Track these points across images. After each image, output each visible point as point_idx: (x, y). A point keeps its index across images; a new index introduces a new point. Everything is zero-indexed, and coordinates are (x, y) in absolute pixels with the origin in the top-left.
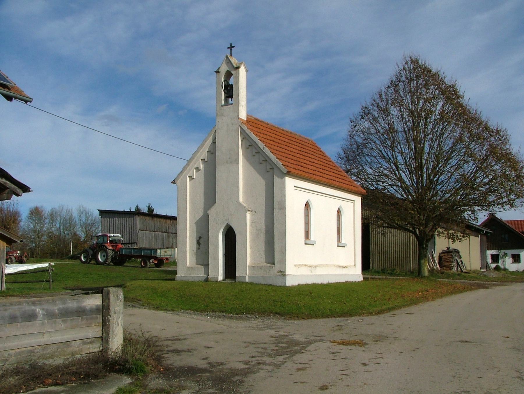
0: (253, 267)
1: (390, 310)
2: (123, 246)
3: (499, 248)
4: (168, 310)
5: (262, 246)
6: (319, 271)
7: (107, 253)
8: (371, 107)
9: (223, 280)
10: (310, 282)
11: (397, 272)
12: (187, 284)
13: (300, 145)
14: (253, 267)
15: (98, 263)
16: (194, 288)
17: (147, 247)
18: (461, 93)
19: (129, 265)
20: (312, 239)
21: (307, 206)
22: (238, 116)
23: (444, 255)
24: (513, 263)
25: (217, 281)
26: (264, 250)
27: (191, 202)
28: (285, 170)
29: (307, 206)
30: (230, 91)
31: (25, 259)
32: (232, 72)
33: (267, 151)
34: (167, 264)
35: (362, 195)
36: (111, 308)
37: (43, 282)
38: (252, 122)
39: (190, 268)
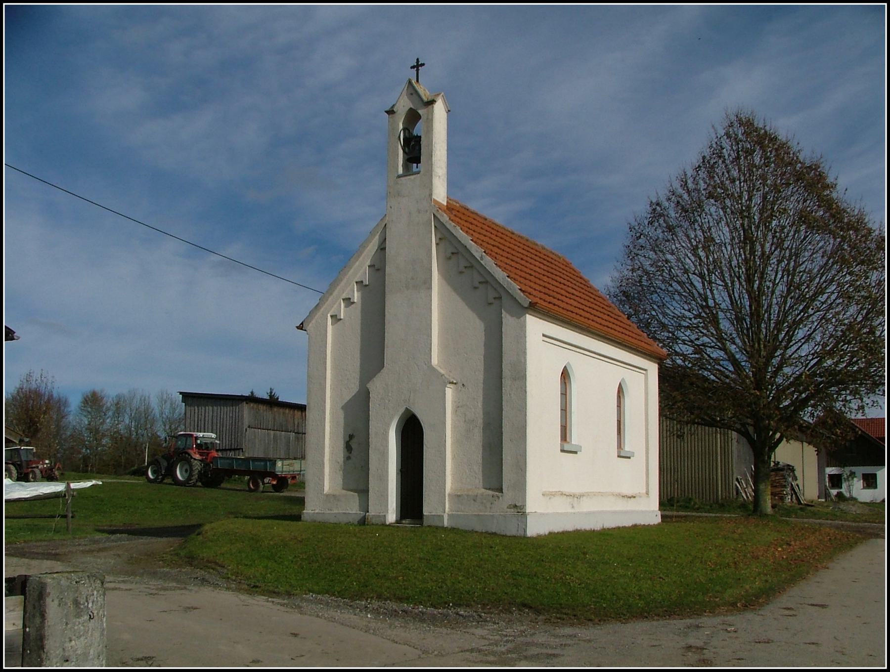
0: (459, 496)
2: (220, 454)
3: (841, 464)
4: (277, 594)
5: (477, 455)
6: (587, 506)
7: (191, 466)
8: (666, 204)
9: (397, 522)
10: (570, 528)
11: (695, 503)
12: (326, 529)
13: (545, 262)
14: (457, 497)
15: (177, 482)
16: (339, 540)
17: (261, 455)
18: (830, 180)
19: (228, 486)
21: (565, 375)
22: (431, 195)
24: (864, 488)
25: (384, 525)
26: (480, 461)
27: (335, 367)
28: (525, 301)
29: (565, 375)
30: (414, 150)
31: (56, 473)
32: (420, 112)
33: (489, 262)
34: (294, 485)
36: (49, 644)
37: (53, 517)
39: (332, 498)
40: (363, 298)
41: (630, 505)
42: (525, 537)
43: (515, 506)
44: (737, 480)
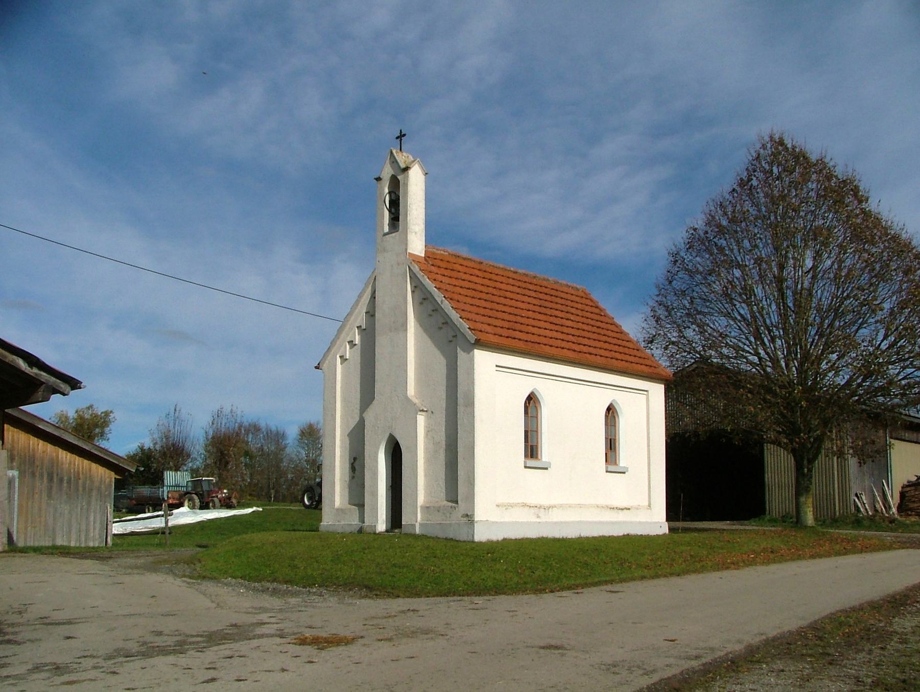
1: (569, 588)
6: (556, 516)
9: (387, 531)
14: (426, 509)
20: (544, 459)
22: (406, 250)
23: (908, 489)
25: (375, 533)
28: (471, 337)
29: (532, 401)
32: (399, 177)
33: (447, 306)
35: (667, 380)
38: (432, 261)
39: (340, 511)
40: (362, 340)
41: (621, 517)
42: (473, 542)
43: (467, 515)
44: (856, 495)
